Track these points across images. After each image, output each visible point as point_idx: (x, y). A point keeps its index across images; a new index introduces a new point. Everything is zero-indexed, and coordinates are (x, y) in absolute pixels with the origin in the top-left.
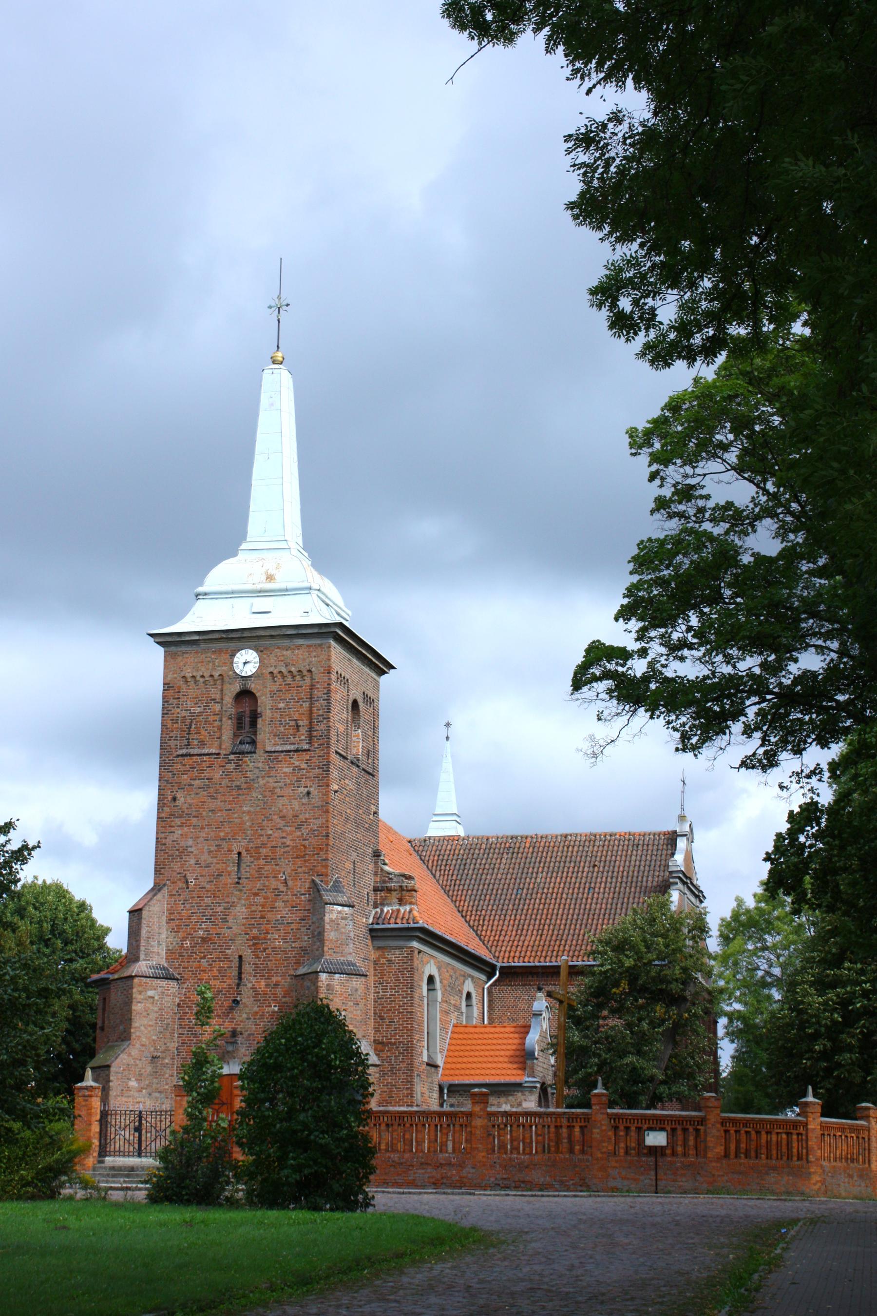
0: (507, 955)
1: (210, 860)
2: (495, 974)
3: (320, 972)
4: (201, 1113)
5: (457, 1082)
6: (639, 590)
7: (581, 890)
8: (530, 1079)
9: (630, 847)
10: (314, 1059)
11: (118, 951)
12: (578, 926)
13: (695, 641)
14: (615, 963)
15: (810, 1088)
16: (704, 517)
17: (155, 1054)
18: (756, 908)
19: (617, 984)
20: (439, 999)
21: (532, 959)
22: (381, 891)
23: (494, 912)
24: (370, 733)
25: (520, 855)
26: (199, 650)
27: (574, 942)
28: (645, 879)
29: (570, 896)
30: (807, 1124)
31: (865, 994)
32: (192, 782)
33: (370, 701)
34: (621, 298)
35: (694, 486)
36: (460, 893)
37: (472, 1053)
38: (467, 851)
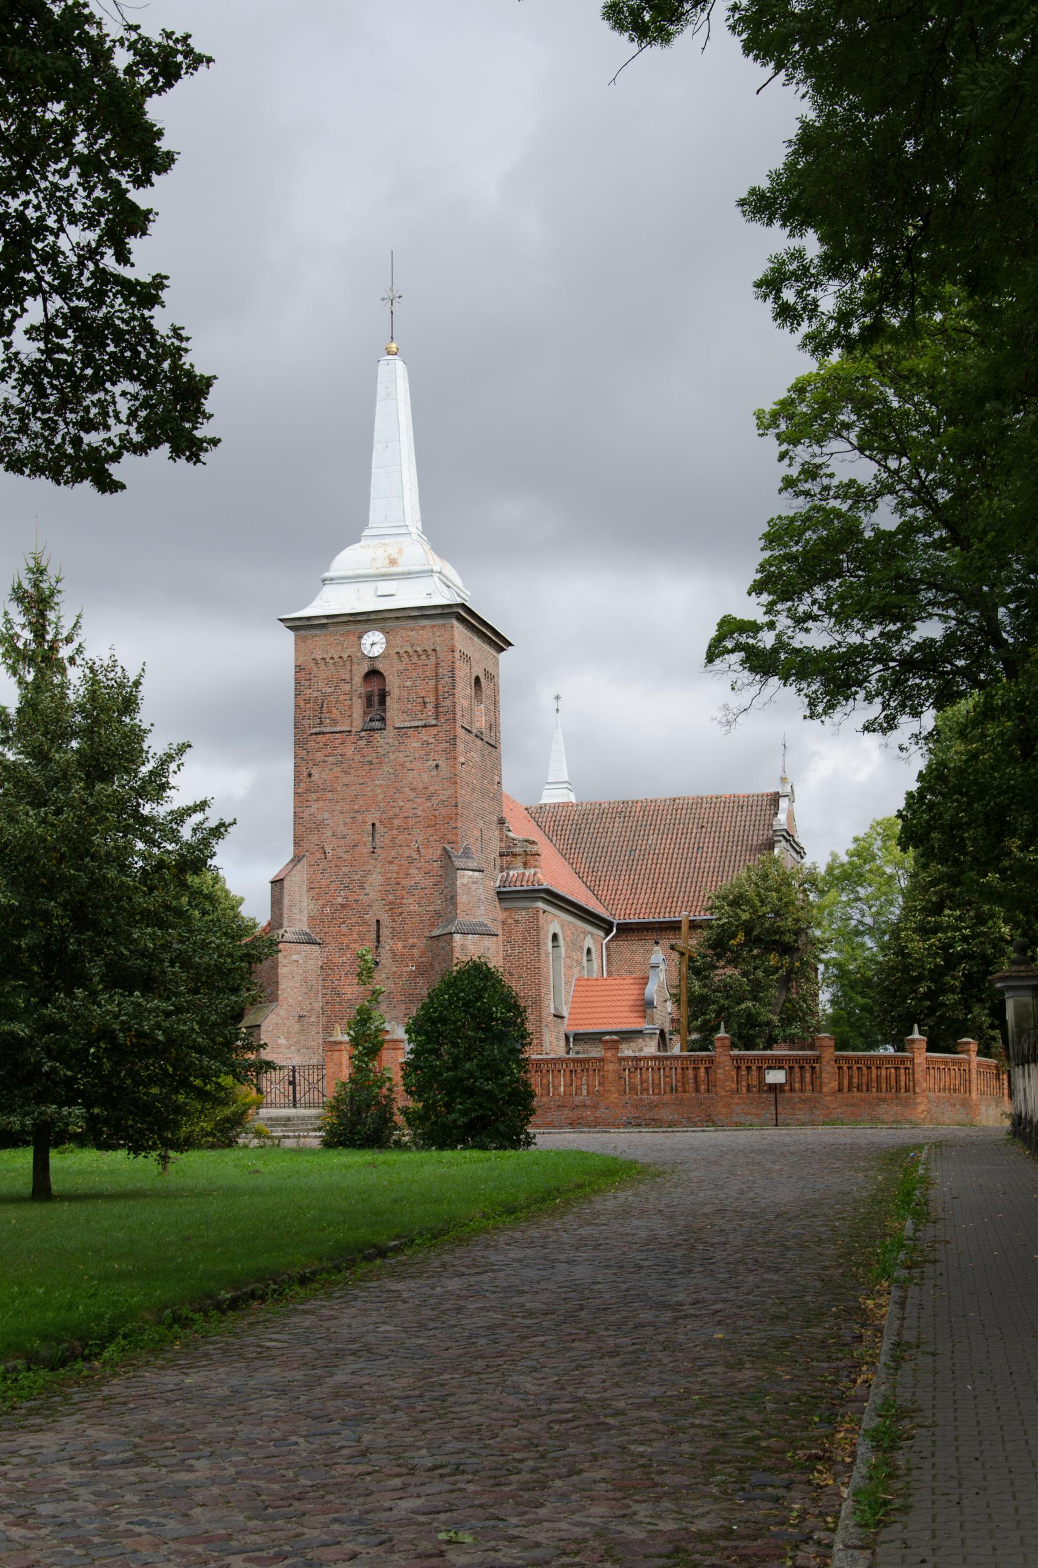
0: (623, 912)
1: (346, 832)
4: (367, 1064)
9: (735, 809)
13: (820, 613)
15: (916, 1026)
19: (734, 936)
20: (563, 955)
24: (492, 708)
27: (686, 899)
29: (680, 856)
31: (965, 939)
33: (491, 677)
34: (784, 290)
37: (595, 1004)
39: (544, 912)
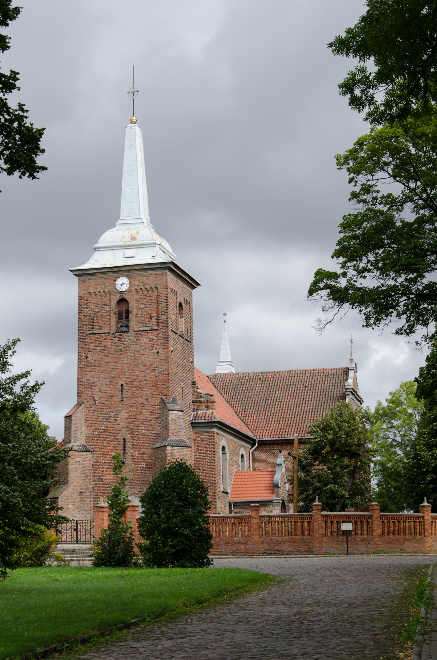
0: (261, 434)
1: (106, 389)
2: (255, 445)
3: (167, 446)
4: (118, 520)
5: (238, 501)
6: (344, 242)
7: (299, 399)
8: (277, 498)
10: (179, 491)
11: (53, 438)
12: (298, 419)
13: (372, 268)
14: (322, 437)
15: (425, 498)
16: (376, 202)
17: (81, 491)
18: (388, 406)
19: (323, 448)
20: (228, 458)
21: (274, 436)
22: (196, 402)
23: (253, 412)
24: (189, 320)
25: (266, 382)
26: (97, 278)
27: (297, 427)
28: (332, 393)
29: (293, 403)
30: (424, 517)
32: (96, 348)
33: (188, 303)
34: (356, 89)
35: (372, 186)
36: (235, 402)
37: (245, 486)
38: (238, 381)
39: (218, 434)
